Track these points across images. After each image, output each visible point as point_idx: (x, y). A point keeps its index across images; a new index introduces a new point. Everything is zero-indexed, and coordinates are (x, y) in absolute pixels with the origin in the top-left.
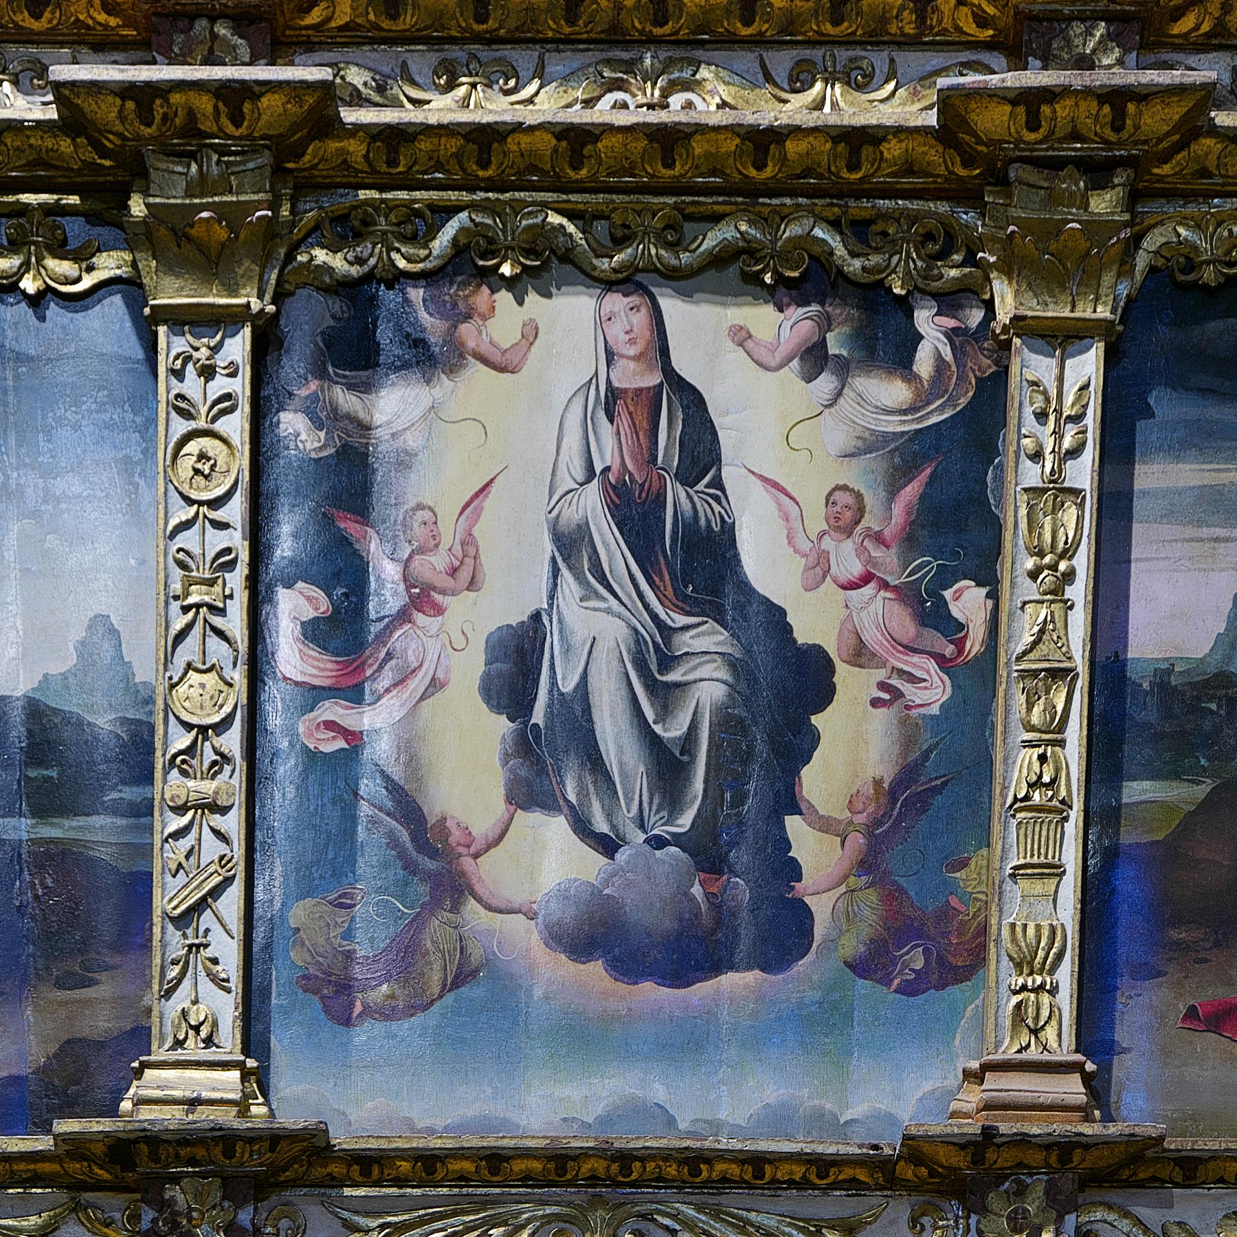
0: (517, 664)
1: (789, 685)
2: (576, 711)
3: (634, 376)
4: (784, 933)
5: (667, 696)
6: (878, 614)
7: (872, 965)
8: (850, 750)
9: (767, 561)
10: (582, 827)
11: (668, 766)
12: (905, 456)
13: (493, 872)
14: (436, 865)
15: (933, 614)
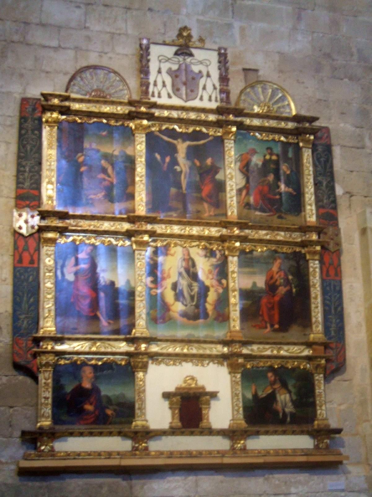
0: (175, 286)
1: (205, 290)
2: (181, 292)
3: (187, 257)
4: (206, 316)
5: (192, 290)
6: (214, 282)
7: (216, 319)
8: (212, 297)
9: (201, 275)
10: (183, 303)
11: (192, 297)
12: (216, 266)
13: (173, 308)
14: (166, 307)
15: (220, 282)
